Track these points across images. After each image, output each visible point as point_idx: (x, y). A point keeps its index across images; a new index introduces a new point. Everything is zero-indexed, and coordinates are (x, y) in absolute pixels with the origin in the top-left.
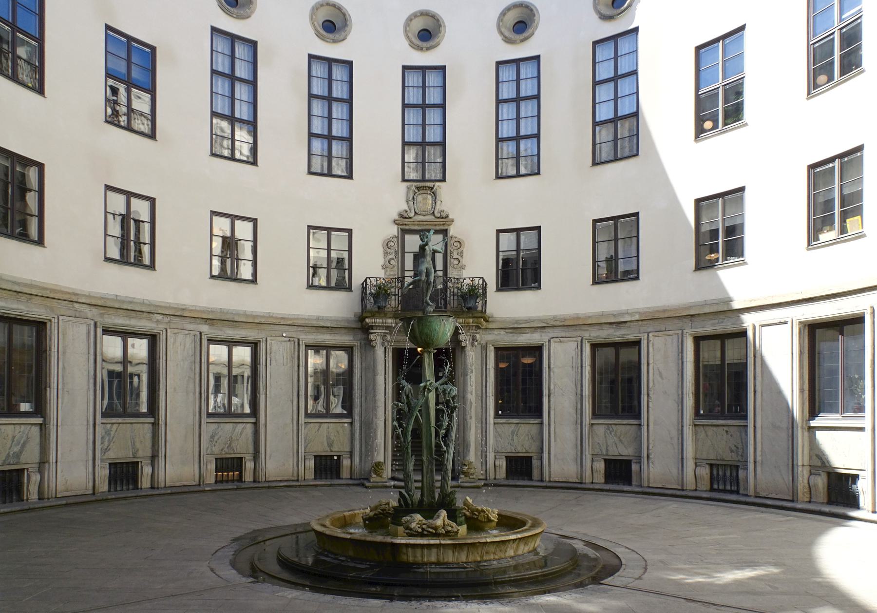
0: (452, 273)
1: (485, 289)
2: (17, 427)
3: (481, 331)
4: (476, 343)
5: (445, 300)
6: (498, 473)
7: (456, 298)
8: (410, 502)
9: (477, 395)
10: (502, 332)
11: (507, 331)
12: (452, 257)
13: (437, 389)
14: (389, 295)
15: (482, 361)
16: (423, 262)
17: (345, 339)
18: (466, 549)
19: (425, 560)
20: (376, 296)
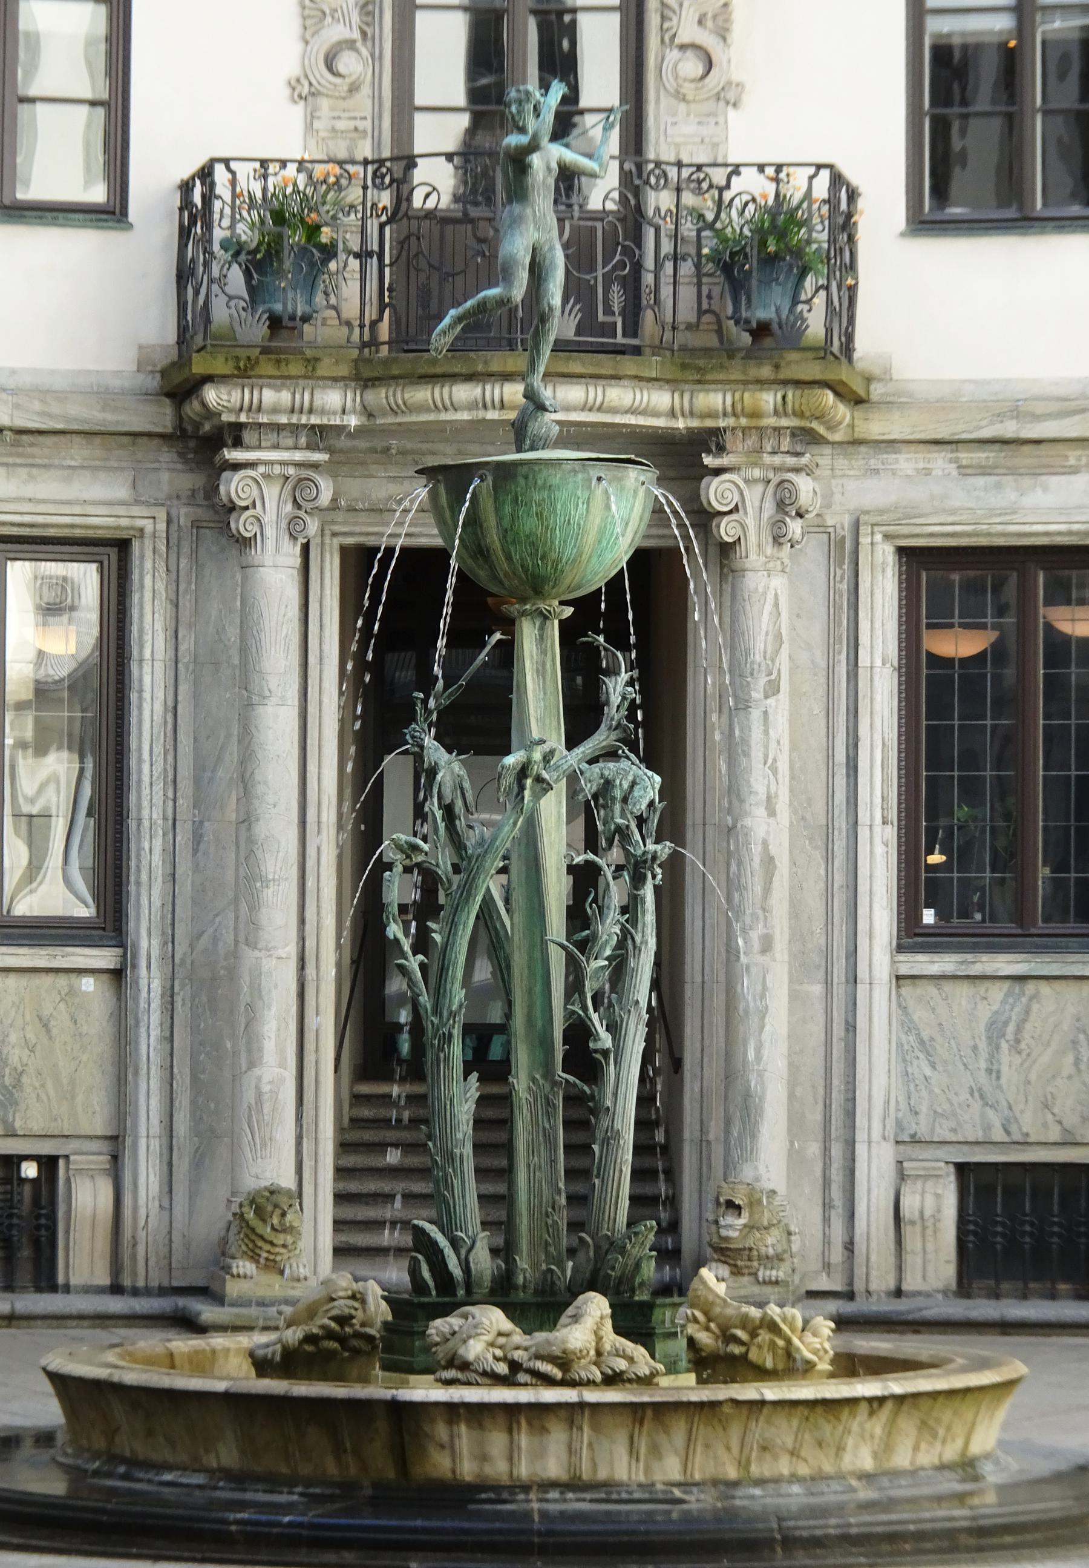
0: (671, 135)
1: (844, 225)
2: (825, 673)
3: (824, 457)
4: (795, 527)
5: (633, 284)
6: (913, 1260)
7: (687, 268)
8: (456, 1271)
9: (800, 818)
10: (940, 461)
11: (966, 456)
12: (669, 40)
13: (573, 779)
14: (329, 252)
15: (832, 621)
16: (517, 221)
17: (89, 495)
18: (679, 1429)
19: (524, 1471)
20: (260, 263)
